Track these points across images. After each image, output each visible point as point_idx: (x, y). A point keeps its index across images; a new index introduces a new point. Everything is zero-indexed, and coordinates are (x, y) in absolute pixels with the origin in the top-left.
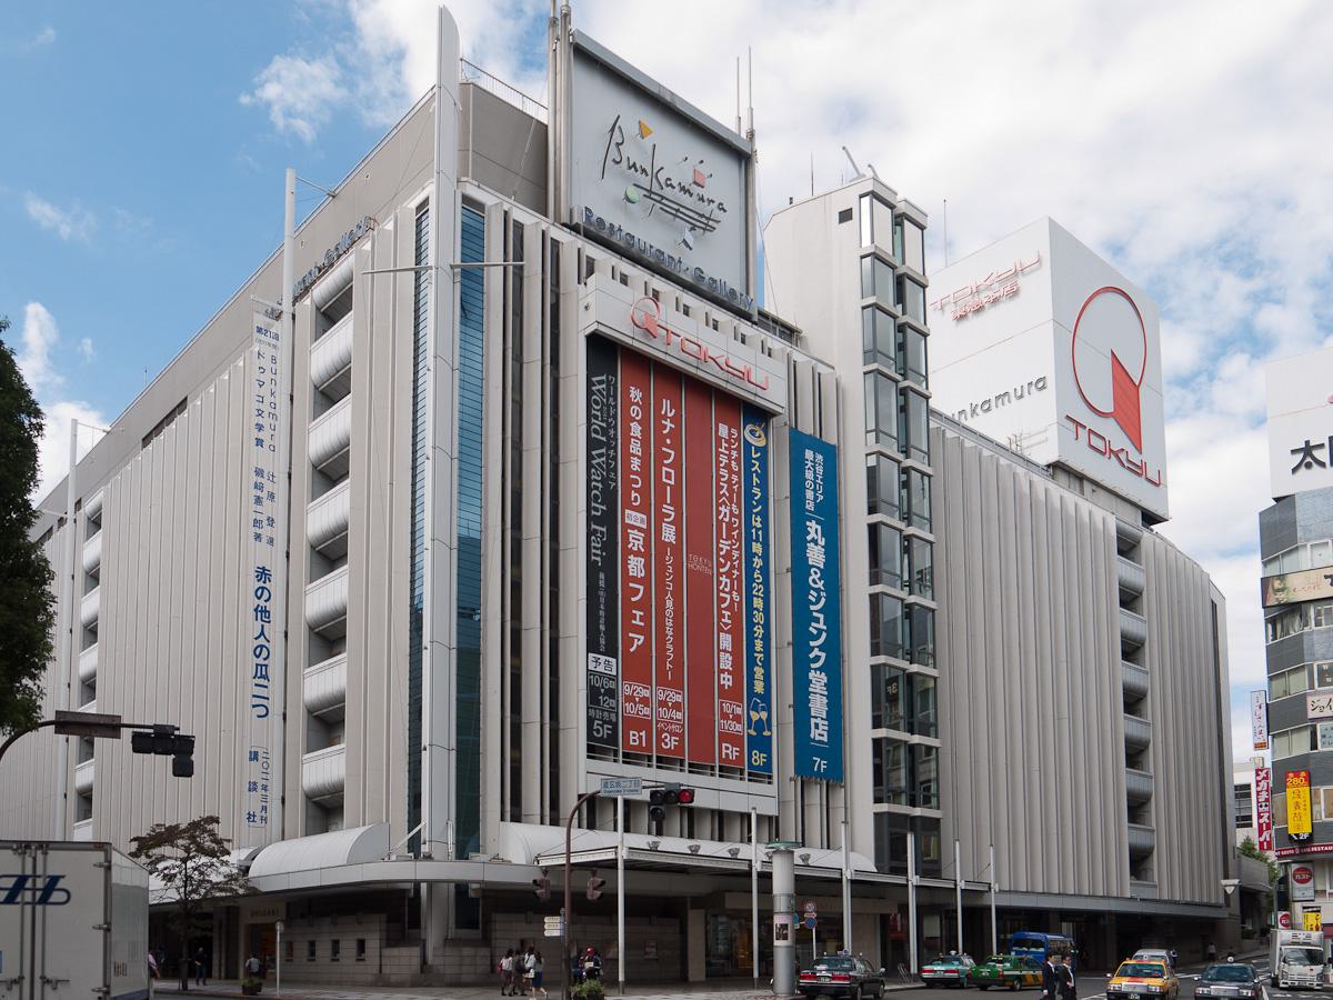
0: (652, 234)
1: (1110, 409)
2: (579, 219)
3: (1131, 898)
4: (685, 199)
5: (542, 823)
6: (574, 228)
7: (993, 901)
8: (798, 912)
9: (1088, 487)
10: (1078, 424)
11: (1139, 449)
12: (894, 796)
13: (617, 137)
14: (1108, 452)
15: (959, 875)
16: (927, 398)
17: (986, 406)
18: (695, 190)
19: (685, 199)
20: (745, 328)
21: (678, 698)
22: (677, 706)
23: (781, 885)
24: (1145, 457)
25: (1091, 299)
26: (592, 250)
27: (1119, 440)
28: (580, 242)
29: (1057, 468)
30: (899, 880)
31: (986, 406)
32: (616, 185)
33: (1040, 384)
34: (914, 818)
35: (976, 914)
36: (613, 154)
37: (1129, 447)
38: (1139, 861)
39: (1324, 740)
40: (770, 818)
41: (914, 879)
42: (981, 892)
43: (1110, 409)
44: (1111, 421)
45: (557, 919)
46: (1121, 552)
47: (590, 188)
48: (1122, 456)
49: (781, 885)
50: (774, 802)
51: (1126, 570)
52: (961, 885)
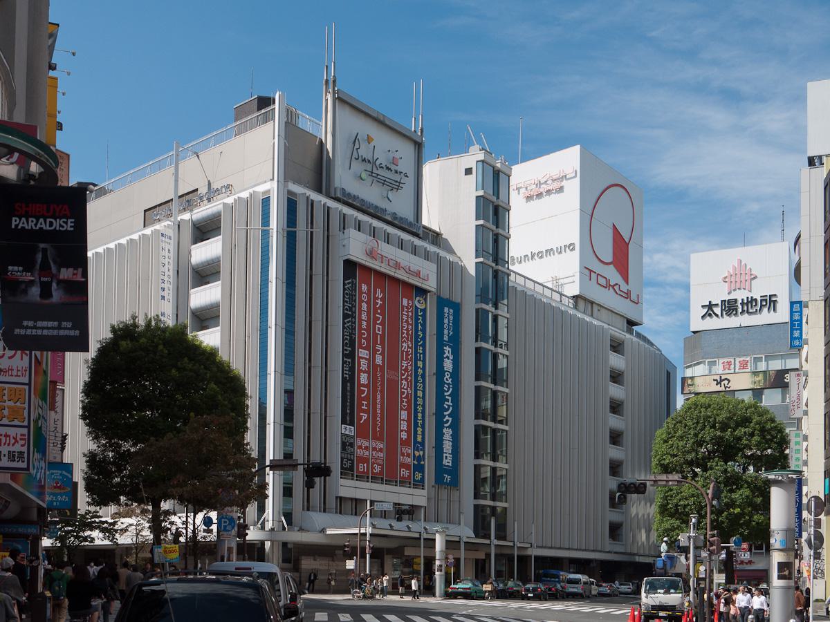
1: (610, 259)
2: (339, 195)
10: (591, 271)
14: (608, 286)
30: (487, 542)
32: (357, 167)
48: (616, 288)
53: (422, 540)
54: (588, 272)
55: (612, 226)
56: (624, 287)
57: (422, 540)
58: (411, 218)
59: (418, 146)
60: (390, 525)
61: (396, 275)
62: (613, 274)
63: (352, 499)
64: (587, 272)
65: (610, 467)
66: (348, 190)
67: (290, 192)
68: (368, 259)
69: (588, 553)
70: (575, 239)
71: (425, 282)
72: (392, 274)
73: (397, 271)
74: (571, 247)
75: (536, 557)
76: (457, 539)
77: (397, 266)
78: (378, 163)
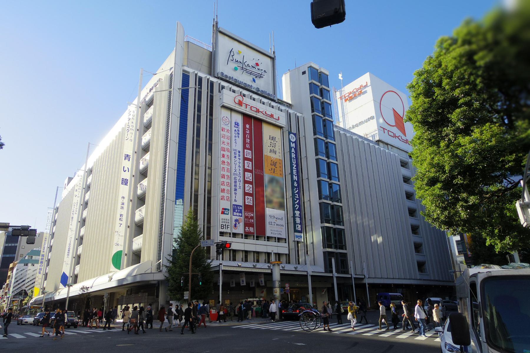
0: (246, 79)
1: (394, 124)
2: (220, 75)
3: (420, 279)
4: (254, 70)
5: (230, 260)
6: (218, 78)
7: (367, 281)
8: (282, 287)
9: (389, 146)
10: (384, 129)
11: (405, 134)
12: (330, 247)
13: (232, 54)
14: (395, 136)
15: (352, 273)
16: (332, 122)
17: (357, 125)
18: (257, 67)
19: (254, 70)
20: (273, 104)
21: (252, 215)
22: (252, 218)
23: (277, 276)
24: (407, 138)
25: (384, 94)
26: (223, 83)
27: (398, 133)
28: (219, 81)
29: (378, 141)
30: (331, 275)
31: (357, 125)
32: (233, 65)
33: (372, 118)
34: (337, 253)
35: (361, 286)
36: (231, 58)
37: (401, 135)
38: (421, 266)
39: (281, 169)
40: (286, 254)
41: (335, 274)
42: (362, 279)
43: (394, 124)
44: (395, 127)
45: (188, 292)
46: (402, 166)
47: (224, 67)
48: (400, 138)
49: (277, 276)
50: (287, 249)
51: (404, 172)
52: (354, 276)
53: (221, 272)
54: (382, 129)
55: (392, 113)
56: (404, 138)
57: (221, 272)
58: (271, 92)
59: (273, 59)
60: (295, 268)
61: (257, 116)
62: (396, 130)
63: (254, 252)
64: (382, 129)
65: (412, 230)
66: (225, 73)
67: (184, 71)
68: (237, 106)
69: (401, 280)
70: (374, 114)
71: (278, 121)
72: (255, 115)
73: (258, 114)
74: (372, 118)
75: (369, 284)
76: (305, 273)
77: (258, 111)
78: (246, 64)
